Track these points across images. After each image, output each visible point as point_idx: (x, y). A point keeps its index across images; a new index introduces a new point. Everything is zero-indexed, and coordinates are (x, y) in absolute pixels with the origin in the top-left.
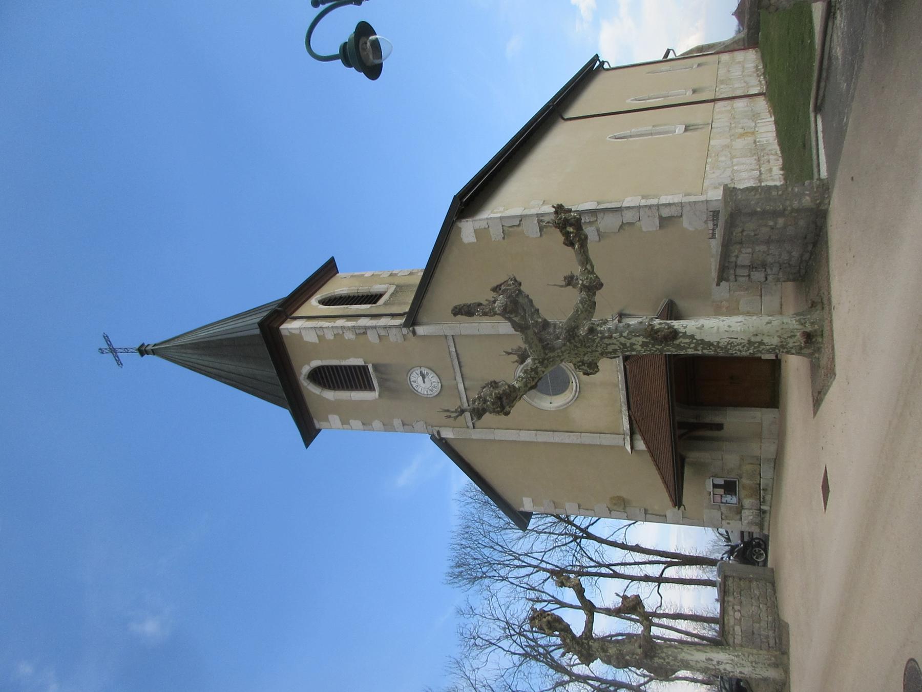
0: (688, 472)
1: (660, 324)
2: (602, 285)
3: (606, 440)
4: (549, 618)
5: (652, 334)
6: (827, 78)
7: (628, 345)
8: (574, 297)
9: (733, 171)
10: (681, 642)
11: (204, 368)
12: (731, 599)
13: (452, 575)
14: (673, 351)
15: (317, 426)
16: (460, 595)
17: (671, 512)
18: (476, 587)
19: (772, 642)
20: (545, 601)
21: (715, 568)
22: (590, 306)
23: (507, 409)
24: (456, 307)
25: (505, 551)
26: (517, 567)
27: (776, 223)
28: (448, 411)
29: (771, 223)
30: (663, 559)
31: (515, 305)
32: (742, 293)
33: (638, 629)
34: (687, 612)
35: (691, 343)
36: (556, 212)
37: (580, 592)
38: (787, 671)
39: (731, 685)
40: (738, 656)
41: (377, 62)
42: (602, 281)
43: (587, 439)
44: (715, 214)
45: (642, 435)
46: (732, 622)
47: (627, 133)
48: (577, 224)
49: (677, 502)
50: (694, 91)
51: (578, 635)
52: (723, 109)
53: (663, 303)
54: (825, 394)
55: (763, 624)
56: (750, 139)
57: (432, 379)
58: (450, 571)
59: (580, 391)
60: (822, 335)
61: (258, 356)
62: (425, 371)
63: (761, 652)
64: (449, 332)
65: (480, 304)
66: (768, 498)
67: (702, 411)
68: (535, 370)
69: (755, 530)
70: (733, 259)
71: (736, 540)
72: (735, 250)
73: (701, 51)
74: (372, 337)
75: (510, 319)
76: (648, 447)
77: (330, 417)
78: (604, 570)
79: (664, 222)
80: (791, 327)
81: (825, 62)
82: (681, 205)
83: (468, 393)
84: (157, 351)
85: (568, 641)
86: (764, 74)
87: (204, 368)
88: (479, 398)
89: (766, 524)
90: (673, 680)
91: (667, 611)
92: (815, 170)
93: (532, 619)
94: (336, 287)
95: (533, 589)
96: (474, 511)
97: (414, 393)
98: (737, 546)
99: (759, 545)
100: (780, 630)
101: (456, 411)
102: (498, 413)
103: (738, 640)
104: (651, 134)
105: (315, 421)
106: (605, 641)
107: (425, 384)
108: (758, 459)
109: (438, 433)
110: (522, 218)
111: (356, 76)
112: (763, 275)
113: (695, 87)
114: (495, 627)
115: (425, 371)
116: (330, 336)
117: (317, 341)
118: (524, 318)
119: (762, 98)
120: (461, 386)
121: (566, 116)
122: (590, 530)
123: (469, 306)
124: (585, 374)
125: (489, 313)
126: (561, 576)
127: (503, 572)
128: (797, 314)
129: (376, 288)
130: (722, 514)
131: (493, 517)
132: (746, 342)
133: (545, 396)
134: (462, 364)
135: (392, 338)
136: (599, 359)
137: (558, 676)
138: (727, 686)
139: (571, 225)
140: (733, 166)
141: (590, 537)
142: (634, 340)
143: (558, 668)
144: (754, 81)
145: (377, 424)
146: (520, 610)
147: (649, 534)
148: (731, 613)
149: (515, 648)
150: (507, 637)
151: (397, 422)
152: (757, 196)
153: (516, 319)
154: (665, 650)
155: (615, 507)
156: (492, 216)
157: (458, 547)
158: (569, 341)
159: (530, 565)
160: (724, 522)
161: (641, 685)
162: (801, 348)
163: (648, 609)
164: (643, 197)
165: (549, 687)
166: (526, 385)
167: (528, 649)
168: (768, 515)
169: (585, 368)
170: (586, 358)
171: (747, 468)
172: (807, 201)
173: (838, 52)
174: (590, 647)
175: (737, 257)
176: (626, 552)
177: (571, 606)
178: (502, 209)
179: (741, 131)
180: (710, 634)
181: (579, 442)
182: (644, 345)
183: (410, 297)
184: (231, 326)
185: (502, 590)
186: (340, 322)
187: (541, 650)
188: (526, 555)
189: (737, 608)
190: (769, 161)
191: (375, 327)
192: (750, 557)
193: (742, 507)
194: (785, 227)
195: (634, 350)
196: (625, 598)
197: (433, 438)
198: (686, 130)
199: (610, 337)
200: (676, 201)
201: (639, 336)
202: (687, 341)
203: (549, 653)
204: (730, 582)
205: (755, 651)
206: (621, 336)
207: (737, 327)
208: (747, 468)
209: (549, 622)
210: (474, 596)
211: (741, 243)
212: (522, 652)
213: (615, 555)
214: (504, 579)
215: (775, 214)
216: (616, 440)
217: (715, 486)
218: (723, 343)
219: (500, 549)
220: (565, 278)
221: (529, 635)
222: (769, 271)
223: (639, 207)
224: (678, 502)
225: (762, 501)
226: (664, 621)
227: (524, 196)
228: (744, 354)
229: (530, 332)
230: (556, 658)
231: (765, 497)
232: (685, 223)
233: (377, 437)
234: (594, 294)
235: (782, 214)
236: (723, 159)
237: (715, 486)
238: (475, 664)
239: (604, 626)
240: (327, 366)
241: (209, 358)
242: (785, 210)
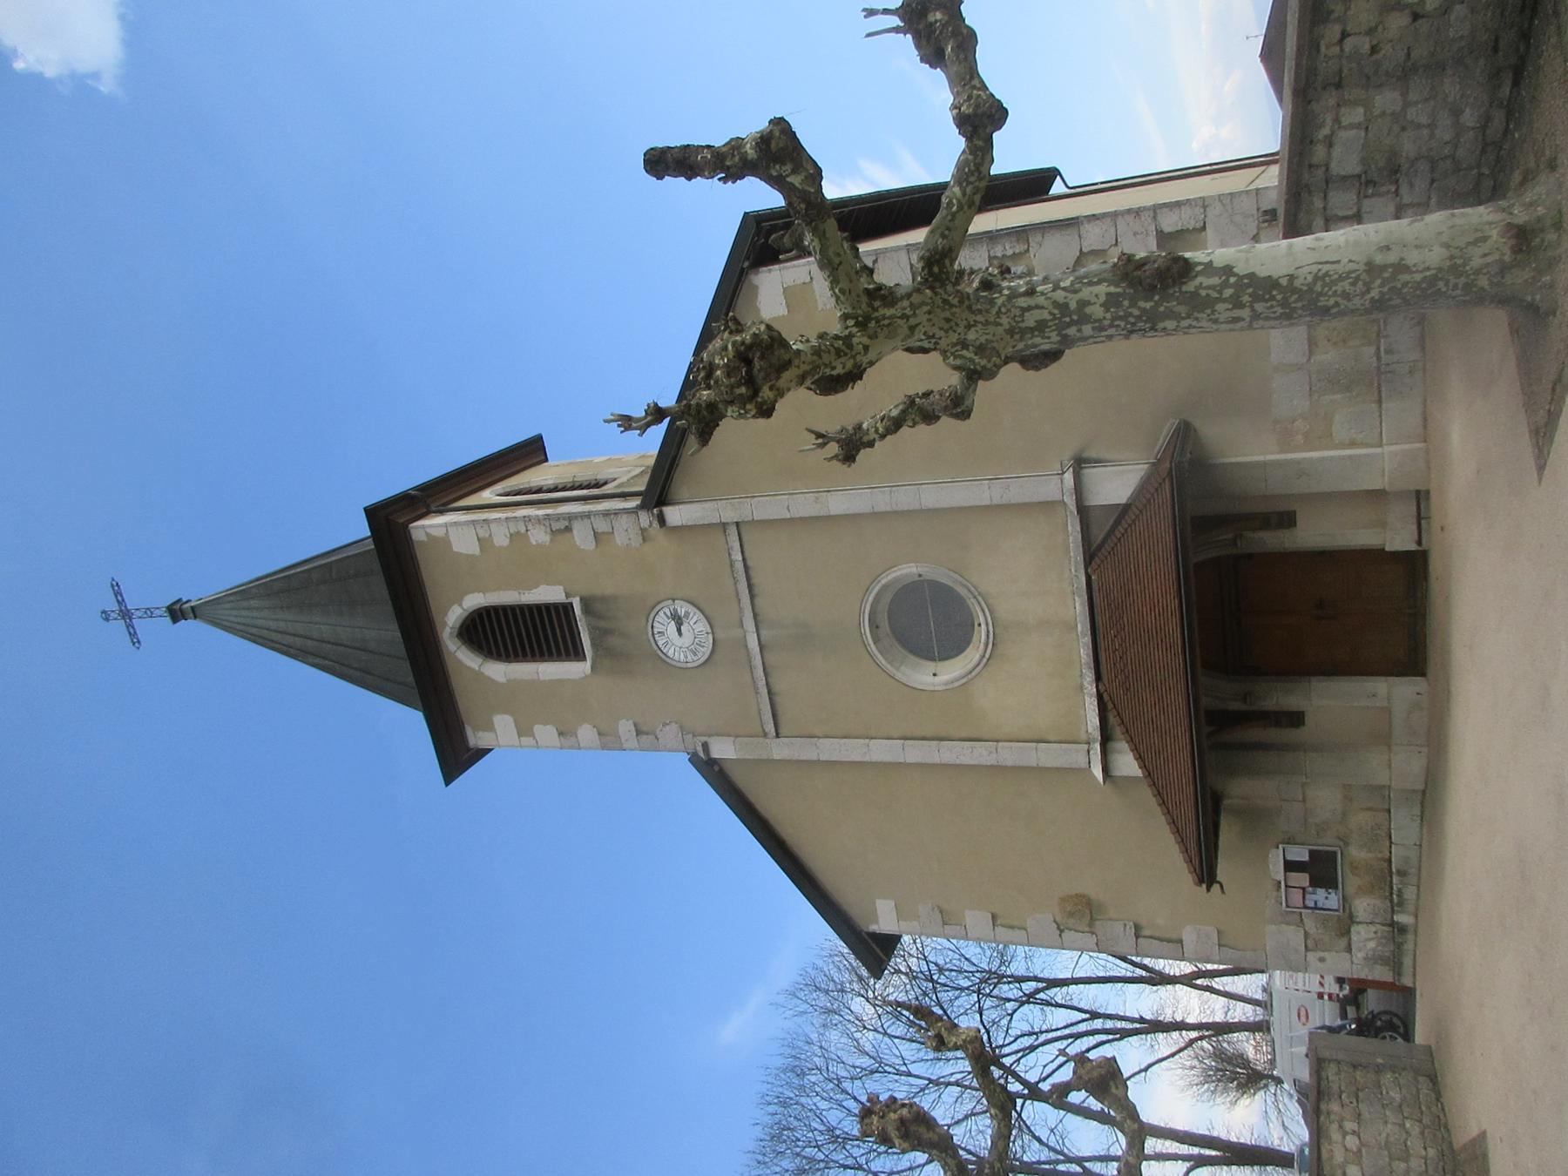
3: (1050, 756)
7: (1073, 306)
12: (1335, 1107)
23: (766, 393)
32: (1338, 397)
43: (1009, 755)
45: (1131, 741)
46: (1339, 1156)
57: (696, 624)
62: (682, 607)
66: (1410, 893)
67: (1256, 647)
74: (582, 536)
82: (1204, 203)
97: (659, 659)
105: (469, 731)
107: (682, 640)
108: (1381, 790)
109: (705, 746)
117: (477, 551)
130: (1306, 934)
132: (1362, 267)
133: (917, 660)
134: (756, 590)
135: (620, 539)
142: (1086, 293)
145: (586, 733)
151: (625, 728)
153: (796, 180)
155: (1071, 922)
160: (1312, 957)
168: (1410, 937)
170: (971, 336)
171: (1360, 819)
181: (989, 760)
182: (1111, 301)
191: (588, 515)
197: (694, 760)
201: (1099, 283)
202: (1215, 281)
204: (1330, 1071)
206: (1056, 287)
208: (1360, 819)
209: (902, 1122)
216: (1073, 756)
217: (1290, 866)
218: (1304, 277)
224: (1206, 874)
225: (1396, 903)
231: (1403, 888)
237: (1290, 866)
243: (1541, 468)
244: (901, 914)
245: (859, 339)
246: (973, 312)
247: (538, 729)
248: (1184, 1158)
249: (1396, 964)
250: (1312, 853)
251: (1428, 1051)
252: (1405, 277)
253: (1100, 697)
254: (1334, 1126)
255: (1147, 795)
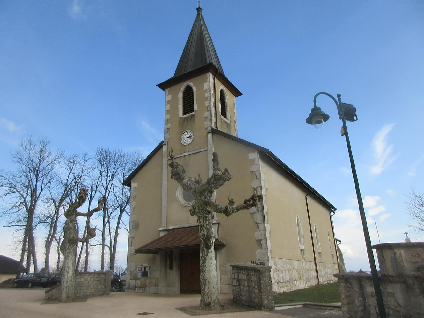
0: (151, 255)
1: (212, 241)
2: (228, 216)
3: (164, 219)
4: (84, 197)
5: (208, 238)
6: (316, 308)
8: (223, 204)
9: (282, 271)
10: (76, 255)
11: (191, 38)
12: (96, 276)
13: (102, 150)
14: (201, 248)
15: (166, 90)
16: (93, 154)
17: (133, 249)
18: (97, 162)
19: (78, 295)
20: (92, 193)
21: (109, 269)
22: (219, 211)
23: (174, 177)
24: (216, 154)
25: (113, 175)
26: (107, 180)
27: (256, 289)
28: (172, 152)
29: (256, 287)
30: (113, 246)
31: (218, 180)
33: (81, 236)
34: (89, 258)
35: (205, 255)
36: (259, 196)
37: (96, 210)
38: (65, 302)
39: (57, 278)
40: (71, 280)
41: (313, 122)
42: (229, 216)
43: (164, 210)
44: (263, 264)
45: (166, 235)
46: (86, 277)
47: (300, 224)
48: (254, 205)
49: (138, 251)
50: (320, 253)
51: (77, 210)
52: (311, 266)
53: (225, 243)
54: (184, 312)
55: (86, 291)
56: (297, 278)
57: (189, 141)
58: (104, 150)
59: (185, 207)
60: (209, 310)
61: (197, 63)
63: (73, 290)
64: (209, 148)
65: (218, 165)
66: (141, 291)
68: (191, 188)
69: (127, 286)
70: (241, 272)
71: (122, 278)
72: (245, 272)
73: (341, 256)
74: (207, 114)
75: (212, 177)
76: (161, 238)
77: (171, 96)
78: (106, 219)
79: (259, 242)
80: (213, 297)
81: (324, 308)
82: (267, 249)
83: (183, 158)
84: (199, 17)
85: (75, 206)
86: (328, 283)
87: (191, 38)
88: (178, 165)
89: (130, 291)
90: (58, 252)
91: (89, 248)
92: (279, 305)
93: (84, 190)
94: (229, 97)
95: (97, 188)
96: (131, 159)
97: (182, 133)
98: (119, 278)
99: (120, 288)
100: (84, 298)
101: (172, 155)
102: (172, 173)
103: (78, 280)
104: (299, 235)
105: (168, 89)
106: (74, 222)
107: (186, 138)
108: (158, 286)
109: (165, 144)
110: (260, 179)
111: (307, 114)
112: (235, 284)
113: (322, 253)
114: (79, 171)
115: (192, 138)
116: (207, 95)
117: (204, 89)
118: (213, 183)
119: (317, 283)
120: (185, 154)
121: (307, 197)
122: (124, 212)
123: (217, 160)
124: (190, 210)
125: (214, 169)
126: (103, 201)
127: (104, 173)
128: (218, 299)
129: (229, 115)
130: (133, 271)
131: (129, 169)
134: (195, 154)
136: (197, 216)
137: (58, 201)
138: (57, 277)
139: (253, 202)
140: (285, 271)
141: (121, 213)
142: (205, 230)
143: (62, 201)
144: (325, 279)
145: (168, 117)
146: (87, 183)
147: (124, 238)
148: (90, 277)
149: (70, 181)
150: (75, 177)
151: (169, 126)
152: (267, 281)
153: (212, 180)
154: (72, 248)
156: (260, 166)
157: (114, 153)
158: (204, 203)
159: (107, 186)
160: (130, 272)
161: (55, 238)
162: (204, 302)
163: (90, 240)
164: (270, 232)
165: (53, 197)
166: (184, 185)
167: (69, 187)
169: (193, 210)
170: (197, 210)
172: (266, 302)
173: (327, 312)
174: (72, 215)
175: (243, 273)
176: (115, 229)
177: (90, 205)
178: (264, 170)
179: (301, 273)
180: (80, 269)
181: (163, 207)
182: (203, 235)
183: (225, 131)
184: (211, 49)
185: (96, 174)
186: (213, 99)
187: (69, 193)
188: (112, 184)
189: (92, 279)
190: (287, 286)
192: (113, 284)
193: (136, 280)
194: (255, 293)
195: (201, 230)
196: (94, 230)
197: (162, 142)
198: (301, 250)
199: (206, 220)
200: (269, 247)
203: (68, 196)
204: (103, 276)
205: (73, 288)
206: (207, 225)
207: (212, 275)
209: (83, 197)
210: (92, 162)
211: (248, 275)
212: (68, 184)
213: (113, 223)
214: (101, 174)
215: (260, 288)
216: (164, 223)
217: (145, 268)
219: (115, 172)
220: (232, 200)
221: (76, 187)
222: (237, 287)
223: (265, 231)
224: (138, 251)
225: (139, 288)
226: (85, 247)
227: (270, 181)
228: (201, 278)
229: (207, 186)
230: (66, 199)
231: (141, 290)
232: (259, 251)
233: (162, 117)
234: (224, 213)
235: (260, 291)
236: (288, 266)
237: (145, 268)
238: (62, 163)
239: (81, 221)
240: (193, 94)
241: (196, 40)
242: (262, 292)
243: (176, 309)
244: (135, 188)
245: (192, 191)
246: (202, 210)
247: (169, 105)
248: (111, 246)
249: (129, 288)
250: (148, 272)
251: (110, 294)
252: (204, 285)
253: (174, 229)
254: (92, 276)
255: (157, 238)
